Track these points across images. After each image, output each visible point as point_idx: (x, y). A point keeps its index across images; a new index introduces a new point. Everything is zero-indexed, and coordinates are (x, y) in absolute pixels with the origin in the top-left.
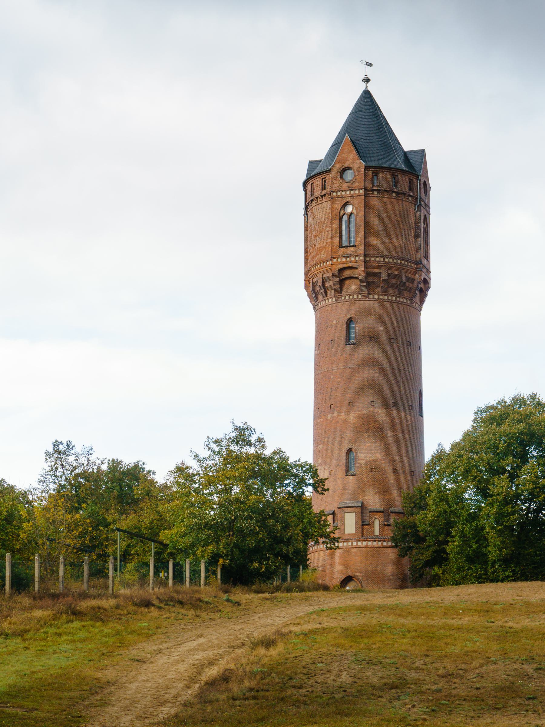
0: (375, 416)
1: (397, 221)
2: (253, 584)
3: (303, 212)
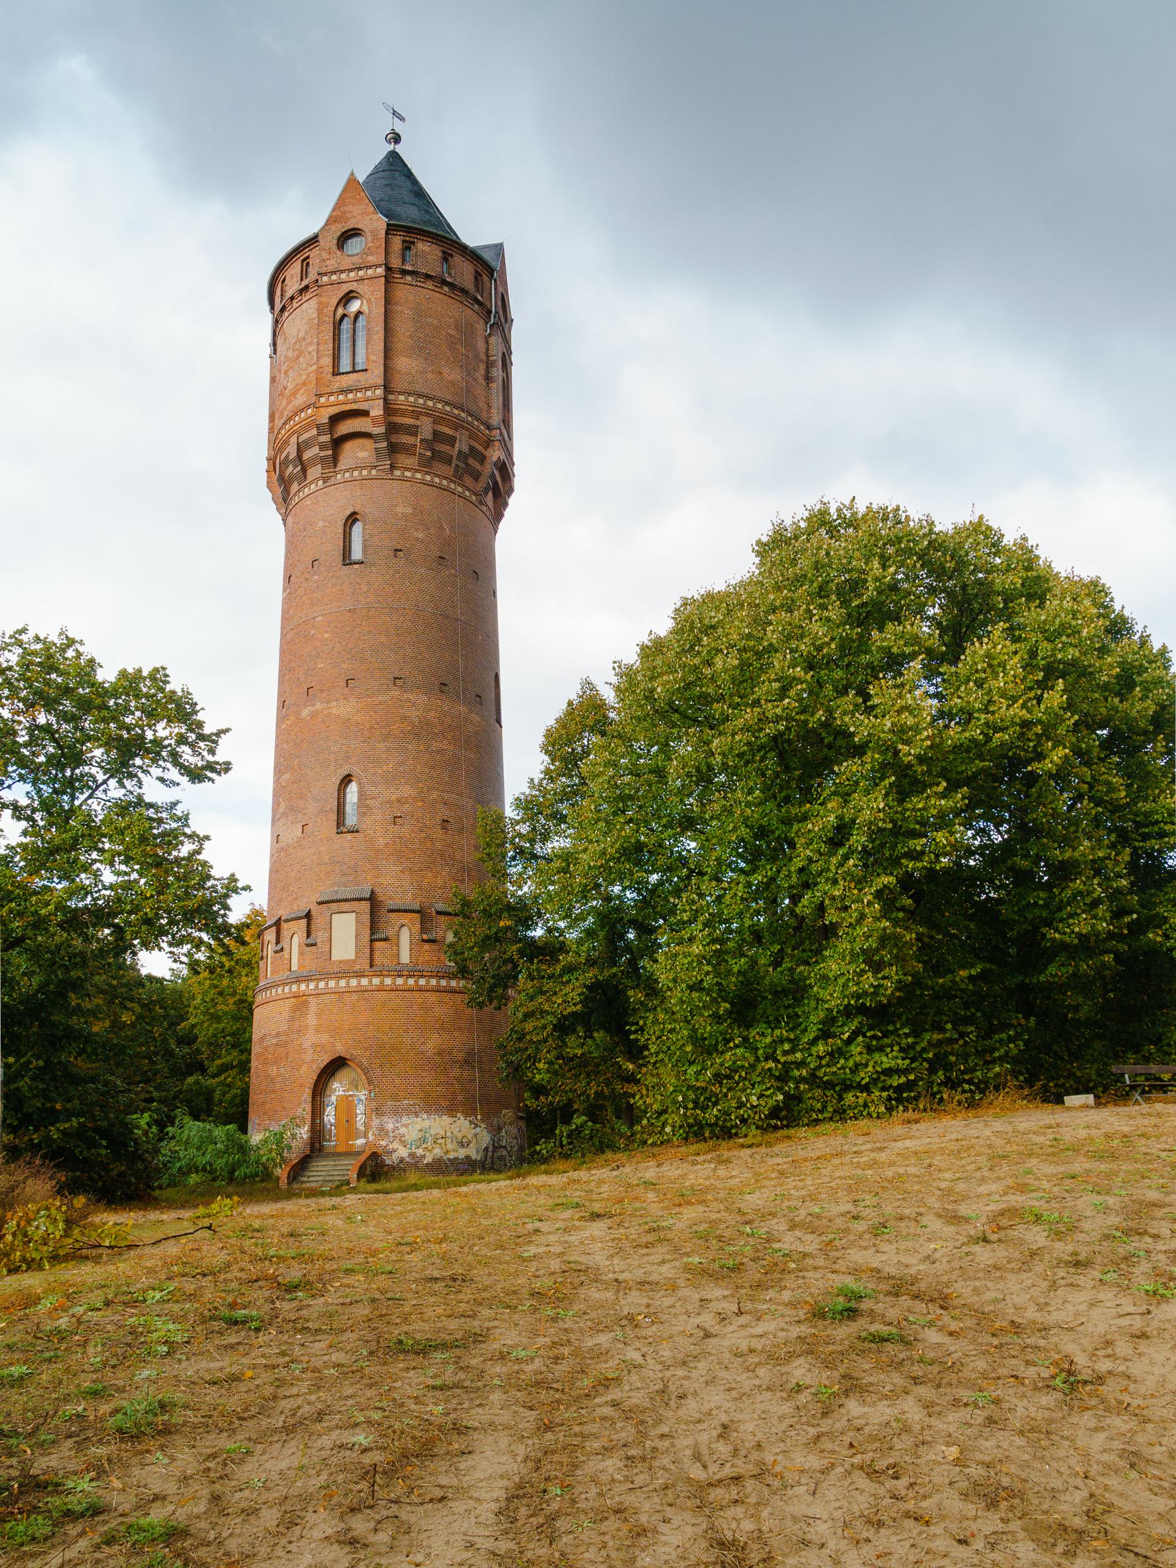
1: (451, 336)
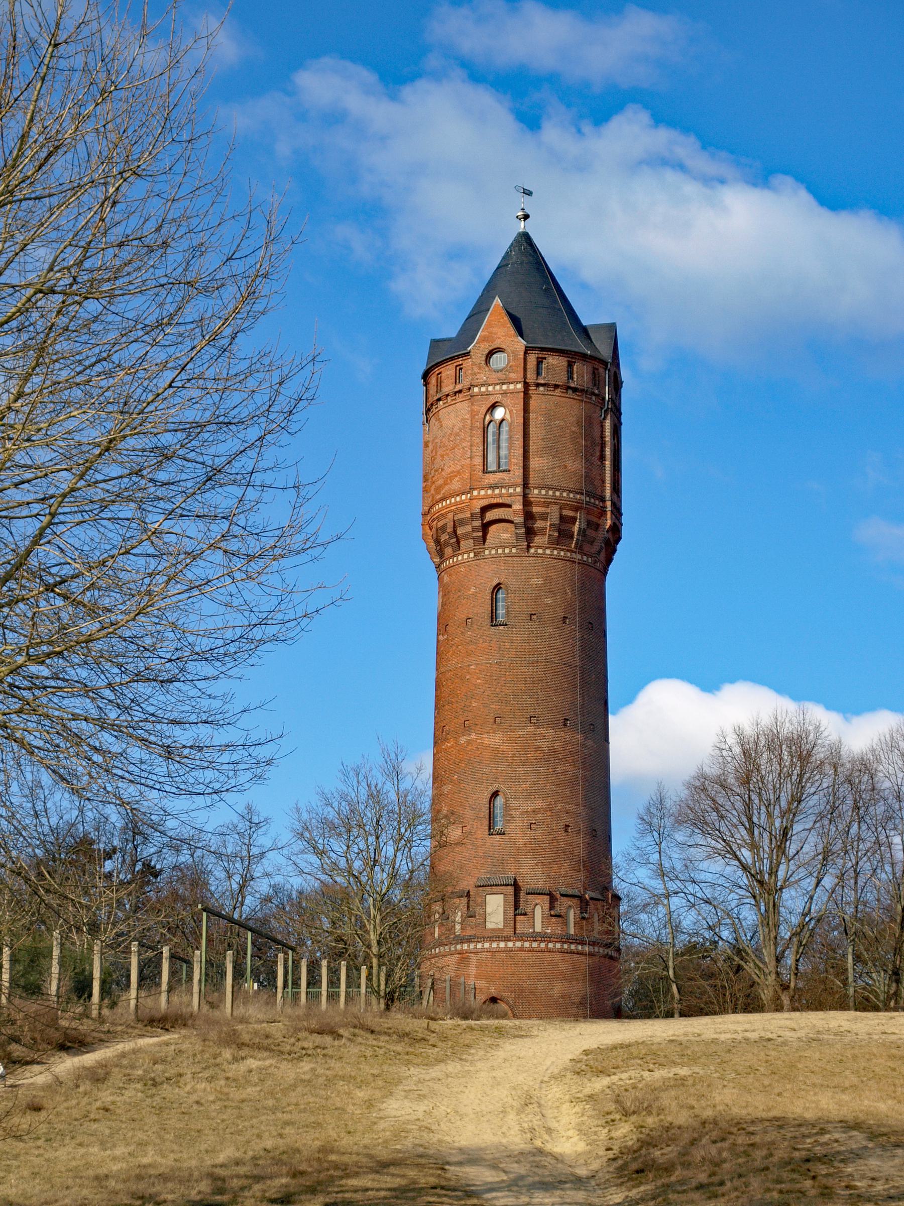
0: (536, 740)
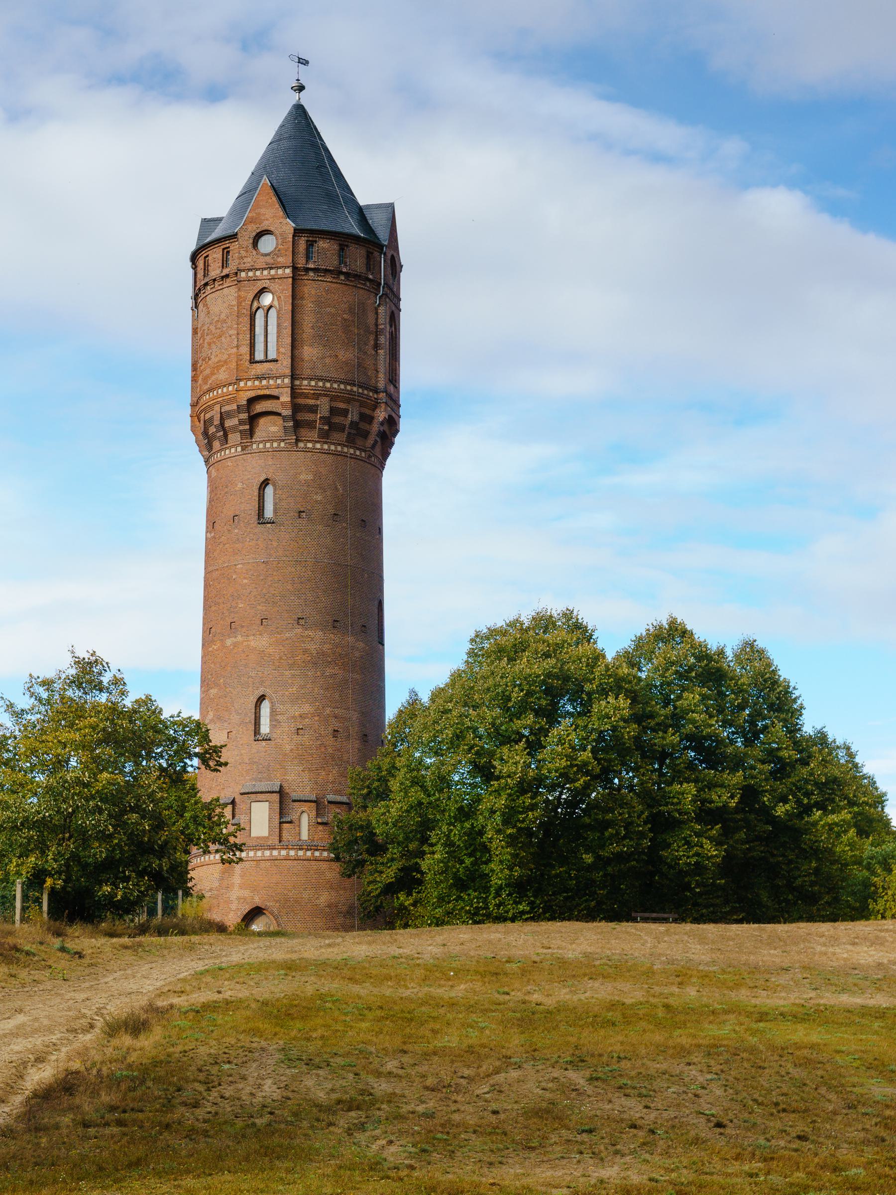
0: (304, 643)
1: (345, 320)
2: (102, 920)
3: (190, 303)
